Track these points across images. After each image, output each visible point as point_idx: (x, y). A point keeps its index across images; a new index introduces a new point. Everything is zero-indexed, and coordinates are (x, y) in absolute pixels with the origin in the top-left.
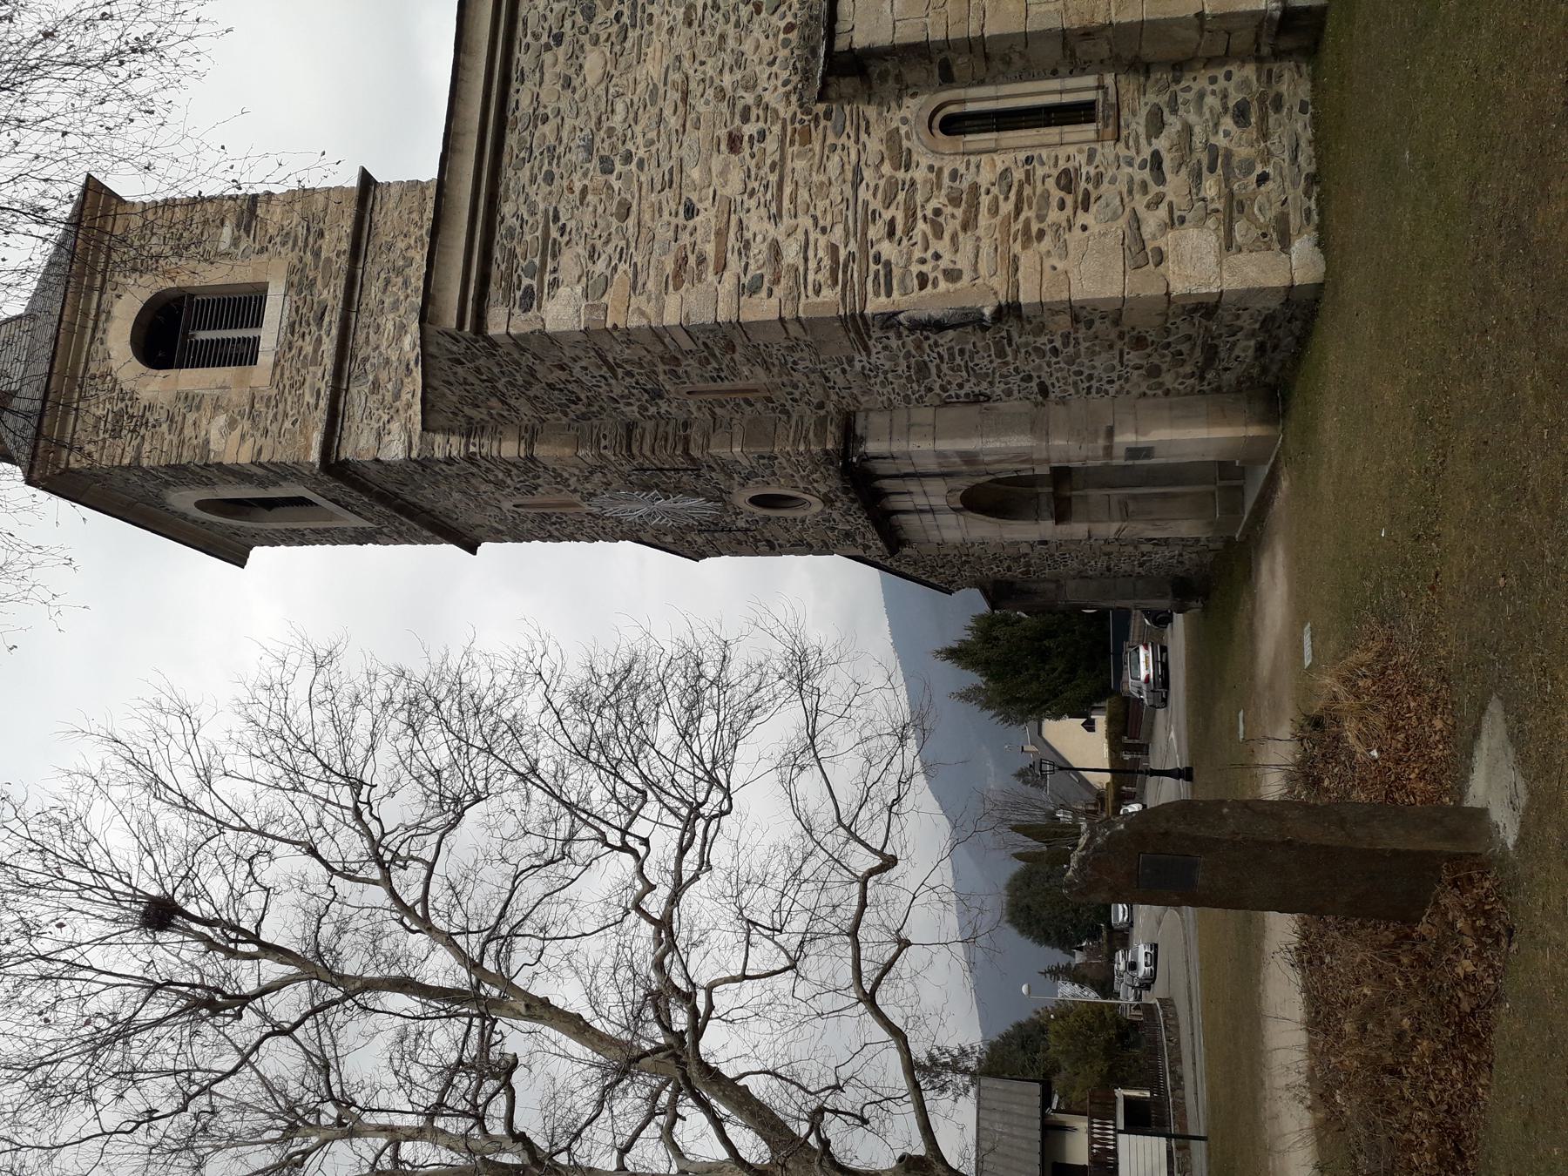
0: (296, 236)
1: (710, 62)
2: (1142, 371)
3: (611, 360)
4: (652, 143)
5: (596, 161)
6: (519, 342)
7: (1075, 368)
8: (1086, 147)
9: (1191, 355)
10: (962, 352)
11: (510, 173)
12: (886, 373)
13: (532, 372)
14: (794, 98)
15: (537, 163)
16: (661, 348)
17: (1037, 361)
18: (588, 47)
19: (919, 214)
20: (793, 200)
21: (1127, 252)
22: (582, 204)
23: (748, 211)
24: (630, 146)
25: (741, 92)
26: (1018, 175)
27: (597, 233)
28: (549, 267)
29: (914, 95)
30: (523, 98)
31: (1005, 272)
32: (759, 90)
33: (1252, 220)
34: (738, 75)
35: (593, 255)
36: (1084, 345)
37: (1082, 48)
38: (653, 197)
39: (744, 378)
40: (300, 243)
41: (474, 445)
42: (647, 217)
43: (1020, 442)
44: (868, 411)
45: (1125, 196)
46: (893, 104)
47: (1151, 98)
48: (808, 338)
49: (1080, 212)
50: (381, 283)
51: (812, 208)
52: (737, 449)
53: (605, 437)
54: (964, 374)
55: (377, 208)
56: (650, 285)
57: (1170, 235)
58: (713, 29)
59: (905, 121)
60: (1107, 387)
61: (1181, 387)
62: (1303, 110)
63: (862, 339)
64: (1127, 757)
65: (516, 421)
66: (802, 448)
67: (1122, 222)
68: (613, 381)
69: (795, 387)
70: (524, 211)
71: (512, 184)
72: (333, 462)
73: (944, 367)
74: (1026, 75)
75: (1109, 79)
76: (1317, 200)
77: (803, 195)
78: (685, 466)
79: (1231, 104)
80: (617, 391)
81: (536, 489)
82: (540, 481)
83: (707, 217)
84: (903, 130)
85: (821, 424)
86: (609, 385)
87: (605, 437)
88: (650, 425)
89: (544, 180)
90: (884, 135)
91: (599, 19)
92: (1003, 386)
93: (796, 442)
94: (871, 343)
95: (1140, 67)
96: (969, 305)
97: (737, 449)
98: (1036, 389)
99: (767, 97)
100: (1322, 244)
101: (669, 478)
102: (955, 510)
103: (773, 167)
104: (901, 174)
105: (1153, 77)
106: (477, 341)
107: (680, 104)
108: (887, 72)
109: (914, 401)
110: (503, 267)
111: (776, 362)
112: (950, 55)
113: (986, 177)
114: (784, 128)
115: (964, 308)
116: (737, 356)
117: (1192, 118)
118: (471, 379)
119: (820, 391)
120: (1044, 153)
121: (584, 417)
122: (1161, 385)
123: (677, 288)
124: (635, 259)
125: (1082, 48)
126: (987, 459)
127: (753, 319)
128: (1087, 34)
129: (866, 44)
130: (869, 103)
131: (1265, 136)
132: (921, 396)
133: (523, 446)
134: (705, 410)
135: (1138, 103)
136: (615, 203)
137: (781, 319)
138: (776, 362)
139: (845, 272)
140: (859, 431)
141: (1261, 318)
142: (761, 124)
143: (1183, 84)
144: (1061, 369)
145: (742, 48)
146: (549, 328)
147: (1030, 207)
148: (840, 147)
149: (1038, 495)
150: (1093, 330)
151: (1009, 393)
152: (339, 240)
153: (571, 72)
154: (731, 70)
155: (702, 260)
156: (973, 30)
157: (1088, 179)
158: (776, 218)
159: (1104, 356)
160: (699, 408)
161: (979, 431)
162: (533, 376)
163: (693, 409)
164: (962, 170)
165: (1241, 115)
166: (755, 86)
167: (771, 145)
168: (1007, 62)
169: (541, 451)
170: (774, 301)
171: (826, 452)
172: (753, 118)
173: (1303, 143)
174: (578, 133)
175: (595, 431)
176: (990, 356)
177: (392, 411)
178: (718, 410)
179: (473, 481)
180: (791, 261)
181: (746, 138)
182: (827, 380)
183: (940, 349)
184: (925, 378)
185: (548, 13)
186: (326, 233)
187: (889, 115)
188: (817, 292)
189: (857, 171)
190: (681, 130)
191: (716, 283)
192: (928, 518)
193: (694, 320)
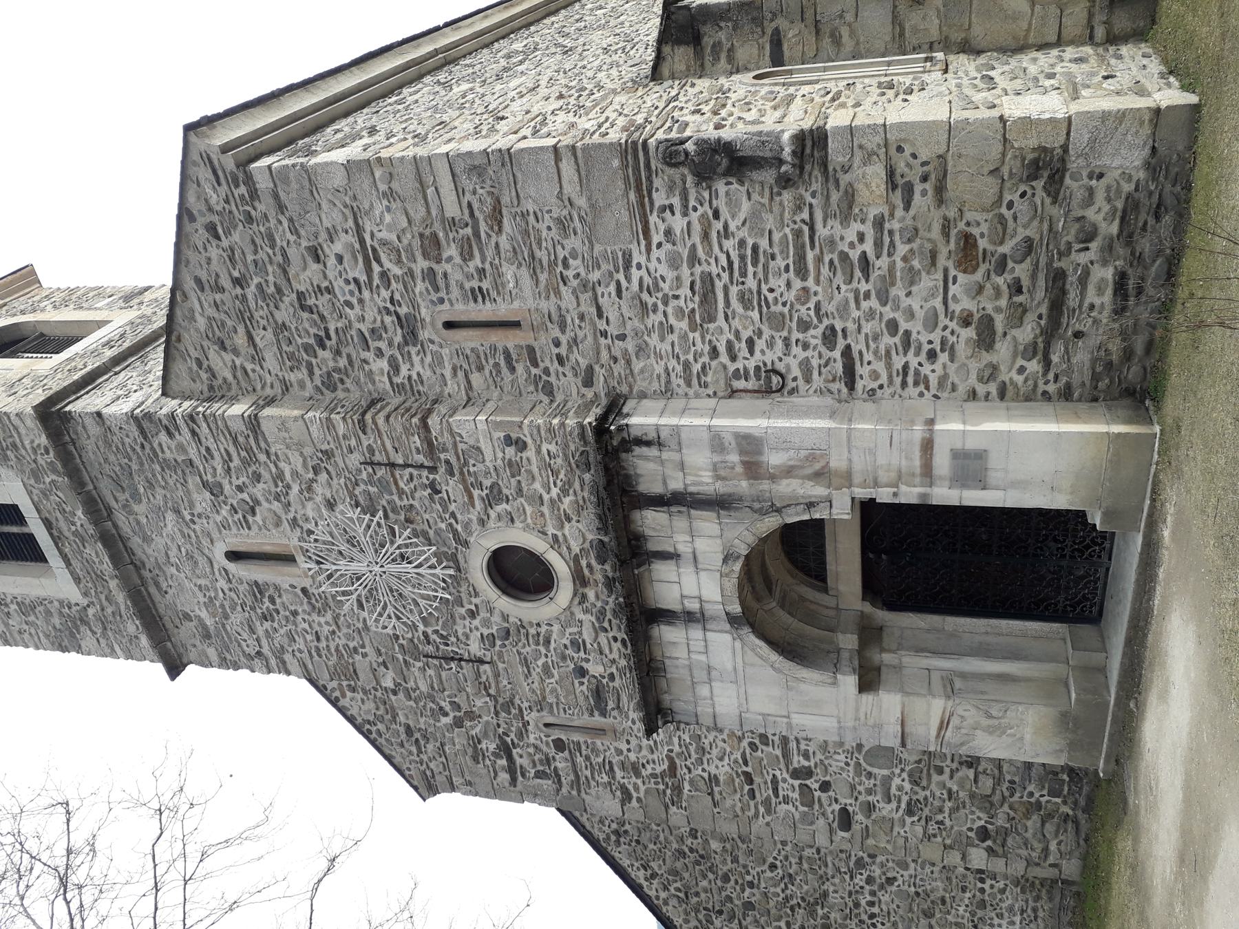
10: (755, 249)
36: (902, 249)
54: (755, 315)
63: (642, 205)
68: (366, 294)
69: (563, 327)
73: (734, 290)
86: (361, 301)
94: (653, 219)
98: (839, 367)
102: (732, 620)
108: (720, 43)
116: (504, 241)
134: (460, 374)
141: (1120, 205)
150: (912, 212)
160: (454, 369)
163: (448, 373)
168: (837, 41)
171: (581, 426)
183: (729, 244)
192: (696, 633)
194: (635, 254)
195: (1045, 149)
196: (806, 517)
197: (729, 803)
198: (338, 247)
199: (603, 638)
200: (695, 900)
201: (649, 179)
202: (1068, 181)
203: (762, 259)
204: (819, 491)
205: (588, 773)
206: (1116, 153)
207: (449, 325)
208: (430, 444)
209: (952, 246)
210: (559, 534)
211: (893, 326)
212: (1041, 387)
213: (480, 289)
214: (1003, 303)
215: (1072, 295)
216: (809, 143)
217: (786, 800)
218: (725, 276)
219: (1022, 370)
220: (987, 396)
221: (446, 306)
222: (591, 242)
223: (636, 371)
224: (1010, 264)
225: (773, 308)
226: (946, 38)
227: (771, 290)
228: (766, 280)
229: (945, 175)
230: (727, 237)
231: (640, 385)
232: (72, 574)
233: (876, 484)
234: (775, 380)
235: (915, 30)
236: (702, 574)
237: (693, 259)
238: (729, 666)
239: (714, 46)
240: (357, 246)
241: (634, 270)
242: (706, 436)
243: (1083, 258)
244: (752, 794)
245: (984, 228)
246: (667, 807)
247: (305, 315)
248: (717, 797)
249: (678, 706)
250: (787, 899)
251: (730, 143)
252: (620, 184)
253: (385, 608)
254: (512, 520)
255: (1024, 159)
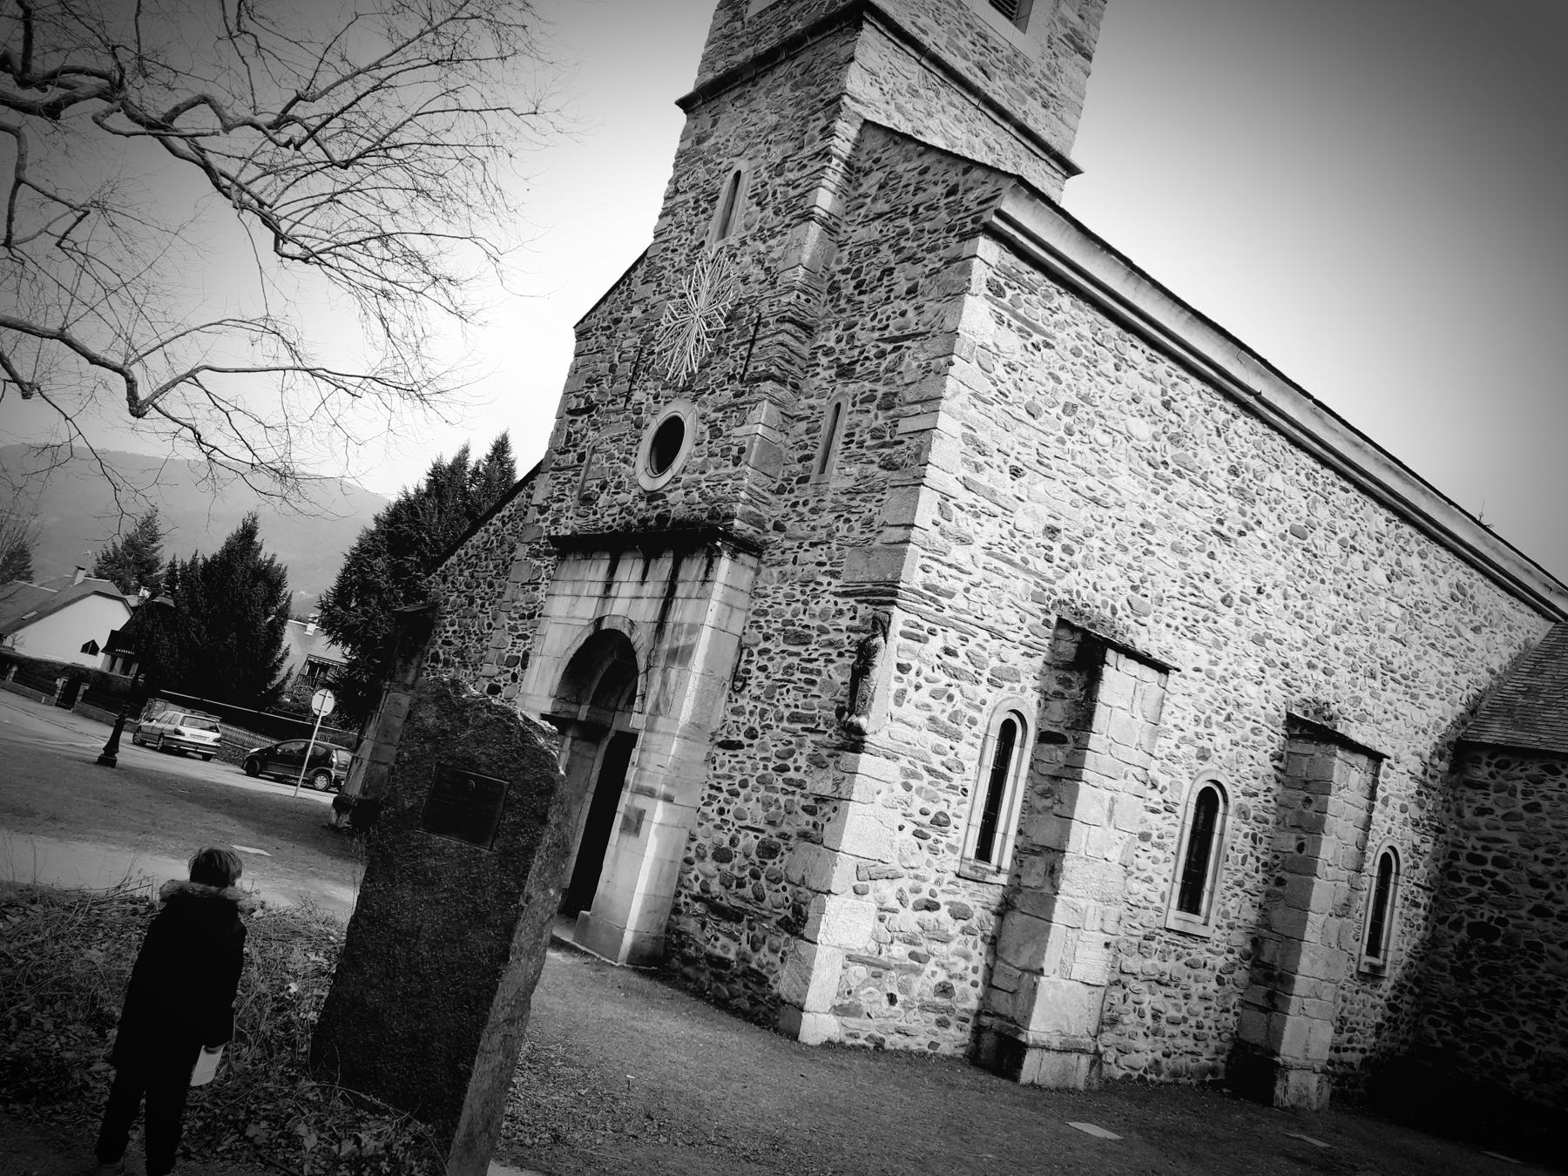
0: (1050, 80)
1: (1112, 532)
2: (726, 844)
3: (906, 343)
4: (1073, 458)
5: (1076, 401)
6: (962, 263)
7: (752, 782)
8: (960, 845)
9: (736, 895)
10: (813, 683)
11: (1090, 317)
12: (805, 603)
13: (913, 259)
14: (1066, 597)
15: (1089, 345)
16: (909, 399)
17: (775, 749)
18: (1154, 429)
19: (954, 681)
20: (997, 570)
21: (872, 863)
22: (1050, 374)
23: (1001, 526)
24: (1077, 436)
25: (1085, 551)
26: (957, 779)
27: (1025, 379)
28: (1015, 323)
29: (1039, 704)
30: (1138, 353)
31: (889, 746)
32: (1081, 568)
33: (865, 984)
34: (1097, 554)
35: (1011, 367)
36: (783, 799)
37: (1040, 864)
38: (1035, 443)
39: (842, 465)
40: (1044, 82)
41: (838, 165)
42: (1022, 430)
43: (686, 709)
44: (758, 572)
45: (915, 871)
46: (1037, 683)
47: (978, 913)
48: (877, 543)
49: (915, 827)
50: (993, 144)
51: (986, 585)
52: (760, 429)
53: (808, 301)
54: (779, 676)
55: (1048, 169)
56: (973, 411)
57: (874, 906)
58: (1133, 544)
59: (1023, 690)
60: (715, 806)
61: (692, 877)
62: (933, 1045)
63: (861, 594)
64: (59, 683)
65: (848, 218)
66: (743, 495)
67: (895, 864)
68: (876, 335)
69: (814, 511)
70: (1059, 317)
71: (1082, 315)
72: (865, 14)
73: (795, 660)
74: (1028, 807)
75: (1003, 879)
76: (864, 1047)
77: (997, 580)
78: (751, 369)
79: (954, 982)
80: (863, 336)
81: (759, 204)
82: (769, 211)
83: (1007, 487)
84: (1017, 686)
85: (758, 522)
86: (873, 329)
87: (808, 301)
88: (805, 351)
89: (1077, 348)
90: (1018, 668)
91: (1169, 447)
92: (748, 709)
93: (750, 491)
94: (852, 601)
95: (1005, 909)
96: (873, 705)
97: (760, 429)
98: (733, 738)
99: (1074, 573)
100: (829, 1045)
101: (736, 347)
102: (599, 621)
103: (1025, 561)
104: (987, 674)
105: (993, 918)
106: (974, 221)
107: (1093, 494)
108: (1070, 687)
109: (755, 618)
110: (1026, 277)
111: (853, 503)
112: (1069, 747)
113: (961, 747)
114: (1049, 581)
115: (872, 700)
116: (874, 468)
117: (954, 945)
118: (921, 197)
119: (800, 533)
120: (967, 807)
121: (834, 288)
122: (702, 858)
123: (964, 435)
124: (996, 404)
125: (1040, 864)
126: (673, 673)
127: (921, 498)
128: (1053, 872)
129: (1104, 678)
130: (1045, 663)
131: (922, 1008)
132: (760, 627)
133: (823, 214)
134: (808, 412)
135: (981, 900)
136: (1041, 405)
137: (912, 526)
138: (853, 503)
139: (931, 599)
140: (741, 556)
141: (764, 971)
142: (1057, 561)
143: (980, 943)
144: (755, 769)
145: (1113, 564)
146: (968, 298)
147: (930, 783)
148: (1021, 625)
149: (579, 704)
150: (800, 812)
151: (737, 711)
152: (1036, 120)
153: (1141, 406)
154: (1102, 549)
155: (978, 468)
156: (1086, 774)
157: (936, 841)
158: (988, 549)
159: (761, 814)
160: (812, 408)
161: (708, 673)
162: (908, 259)
163: (812, 401)
164: (975, 729)
165: (945, 990)
166: (1084, 565)
167: (1041, 565)
168: (1044, 794)
169: (814, 229)
170: (929, 525)
172: (1064, 556)
173: (908, 1041)
174: (1100, 393)
175: (815, 293)
176: (796, 706)
177: (888, 96)
178: (803, 425)
179: (790, 145)
180: (953, 551)
181: (1051, 544)
182: (813, 545)
183: (821, 662)
184: (785, 639)
185: (1185, 403)
186: (1044, 110)
187: (1031, 677)
188: (923, 568)
189: (1001, 636)
190: (1074, 487)
191: (957, 475)
192: (598, 589)
193: (936, 444)
194: (840, 582)
195: (805, 921)
196: (638, 693)
197: (521, 596)
198: (911, 314)
199: (616, 510)
200: (483, 556)
201: (872, 603)
202: (787, 935)
203: (806, 687)
204: (649, 706)
205: (561, 480)
206: (790, 975)
207: (838, 406)
208: (758, 380)
209: (775, 839)
210: (680, 485)
211: (744, 784)
212: (685, 892)
213: (852, 441)
214: (736, 872)
215: (726, 925)
216: (857, 738)
217: (514, 644)
218: (805, 655)
219: (697, 878)
220: (689, 849)
221: (850, 409)
222: (852, 545)
223: (773, 569)
224: (754, 882)
225: (778, 691)
226: (1020, 891)
227: (788, 691)
228: (794, 688)
229: (813, 842)
230: (826, 661)
231: (765, 570)
232: (765, 10)
233: (643, 750)
234: (739, 684)
235: (1032, 865)
236: (628, 601)
237: (823, 631)
238: (576, 613)
239: (1070, 681)
240: (906, 332)
241: (828, 579)
242: (699, 621)
243: (744, 938)
244: (522, 617)
245: (778, 866)
246: (529, 543)
247: (878, 274)
248: (527, 587)
249: (566, 564)
250: (469, 634)
251: (868, 673)
252: (876, 578)
253: (675, 319)
254: (697, 445)
255: (804, 904)
